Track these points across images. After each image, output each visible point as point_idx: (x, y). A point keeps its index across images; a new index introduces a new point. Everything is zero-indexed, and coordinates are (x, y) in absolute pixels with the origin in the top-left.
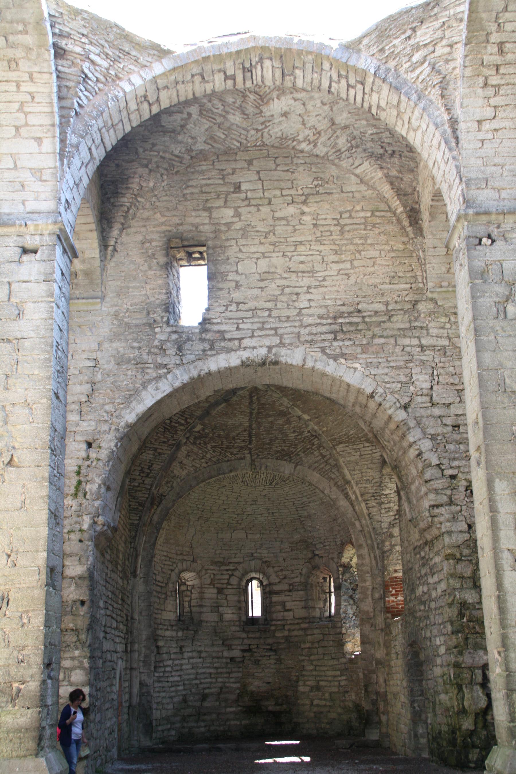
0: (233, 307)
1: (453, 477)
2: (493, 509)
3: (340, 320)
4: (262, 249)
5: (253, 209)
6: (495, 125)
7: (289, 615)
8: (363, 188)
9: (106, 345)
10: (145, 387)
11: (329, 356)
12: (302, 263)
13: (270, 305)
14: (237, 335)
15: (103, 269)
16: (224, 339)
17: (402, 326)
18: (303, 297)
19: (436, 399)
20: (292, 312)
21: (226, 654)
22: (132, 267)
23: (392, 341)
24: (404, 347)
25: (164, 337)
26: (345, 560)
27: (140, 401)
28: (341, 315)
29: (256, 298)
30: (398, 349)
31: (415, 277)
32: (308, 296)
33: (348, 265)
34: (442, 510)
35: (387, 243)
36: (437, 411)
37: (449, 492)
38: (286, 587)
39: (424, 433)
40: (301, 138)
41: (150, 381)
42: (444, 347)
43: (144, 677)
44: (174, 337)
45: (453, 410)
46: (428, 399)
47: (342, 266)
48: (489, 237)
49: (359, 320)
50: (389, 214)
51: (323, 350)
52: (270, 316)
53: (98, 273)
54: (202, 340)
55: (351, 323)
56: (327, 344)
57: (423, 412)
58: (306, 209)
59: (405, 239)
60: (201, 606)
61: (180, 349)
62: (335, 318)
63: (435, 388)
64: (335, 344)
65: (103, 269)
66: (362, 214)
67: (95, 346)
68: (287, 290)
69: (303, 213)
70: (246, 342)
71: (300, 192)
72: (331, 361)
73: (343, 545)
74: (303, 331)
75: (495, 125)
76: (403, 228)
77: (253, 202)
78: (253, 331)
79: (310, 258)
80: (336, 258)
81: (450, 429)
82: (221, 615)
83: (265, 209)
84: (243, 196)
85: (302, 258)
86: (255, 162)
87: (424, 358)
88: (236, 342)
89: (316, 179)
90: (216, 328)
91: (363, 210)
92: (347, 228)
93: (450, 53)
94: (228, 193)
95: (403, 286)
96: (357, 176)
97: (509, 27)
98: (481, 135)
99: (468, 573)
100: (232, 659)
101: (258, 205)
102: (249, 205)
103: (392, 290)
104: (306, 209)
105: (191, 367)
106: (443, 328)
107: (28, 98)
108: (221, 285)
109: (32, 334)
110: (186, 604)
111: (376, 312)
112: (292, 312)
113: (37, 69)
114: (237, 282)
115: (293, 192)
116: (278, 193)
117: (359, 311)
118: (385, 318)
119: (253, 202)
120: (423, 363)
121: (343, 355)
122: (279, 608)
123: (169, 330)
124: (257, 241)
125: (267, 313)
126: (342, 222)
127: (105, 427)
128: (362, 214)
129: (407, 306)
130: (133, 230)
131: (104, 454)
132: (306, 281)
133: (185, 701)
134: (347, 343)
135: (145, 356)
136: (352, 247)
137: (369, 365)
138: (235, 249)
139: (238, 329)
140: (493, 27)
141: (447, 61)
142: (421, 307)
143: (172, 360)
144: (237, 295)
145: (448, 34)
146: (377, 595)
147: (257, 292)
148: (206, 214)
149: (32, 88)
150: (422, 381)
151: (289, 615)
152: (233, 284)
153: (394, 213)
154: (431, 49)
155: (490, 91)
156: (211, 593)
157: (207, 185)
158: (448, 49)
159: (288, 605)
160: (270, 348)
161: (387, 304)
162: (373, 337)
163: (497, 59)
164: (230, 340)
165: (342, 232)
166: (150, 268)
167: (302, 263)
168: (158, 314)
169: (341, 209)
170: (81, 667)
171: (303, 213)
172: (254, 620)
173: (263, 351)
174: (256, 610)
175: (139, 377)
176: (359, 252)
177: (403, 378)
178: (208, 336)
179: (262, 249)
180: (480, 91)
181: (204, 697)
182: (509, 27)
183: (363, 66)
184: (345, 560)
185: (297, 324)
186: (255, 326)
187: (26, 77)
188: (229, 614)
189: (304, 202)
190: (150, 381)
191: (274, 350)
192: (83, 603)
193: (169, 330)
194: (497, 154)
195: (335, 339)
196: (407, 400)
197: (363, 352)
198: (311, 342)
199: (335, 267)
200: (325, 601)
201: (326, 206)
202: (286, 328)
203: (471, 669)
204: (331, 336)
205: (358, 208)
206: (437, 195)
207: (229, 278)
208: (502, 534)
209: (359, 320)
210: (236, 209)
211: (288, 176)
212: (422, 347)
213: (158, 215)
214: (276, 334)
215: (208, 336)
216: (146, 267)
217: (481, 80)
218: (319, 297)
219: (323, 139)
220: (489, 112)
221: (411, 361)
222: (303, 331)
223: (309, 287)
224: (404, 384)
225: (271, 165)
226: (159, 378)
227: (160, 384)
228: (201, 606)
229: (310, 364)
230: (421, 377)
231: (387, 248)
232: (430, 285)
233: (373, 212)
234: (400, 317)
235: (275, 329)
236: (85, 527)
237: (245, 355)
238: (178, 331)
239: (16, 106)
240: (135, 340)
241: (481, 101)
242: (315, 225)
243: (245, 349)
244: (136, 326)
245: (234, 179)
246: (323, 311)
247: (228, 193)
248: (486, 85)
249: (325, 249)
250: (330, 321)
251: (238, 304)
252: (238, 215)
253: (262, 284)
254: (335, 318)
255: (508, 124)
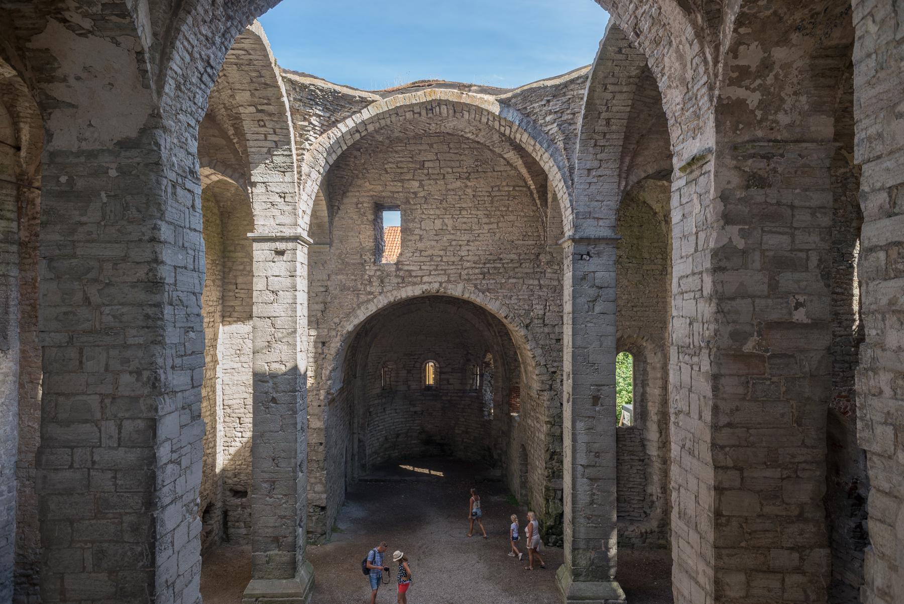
0: (417, 254)
1: (554, 372)
2: (574, 440)
3: (488, 265)
4: (438, 212)
5: (432, 182)
6: (599, 172)
7: (451, 387)
8: (508, 168)
9: (333, 277)
10: (359, 308)
11: (480, 290)
12: (465, 223)
13: (442, 253)
14: (420, 273)
15: (331, 222)
16: (411, 276)
17: (528, 271)
18: (463, 248)
19: (547, 322)
20: (456, 259)
21: (412, 409)
22: (350, 221)
23: (521, 281)
24: (529, 285)
25: (372, 273)
26: (486, 360)
27: (357, 317)
28: (489, 262)
29: (432, 247)
30: (525, 287)
31: (539, 236)
32: (468, 248)
33: (495, 226)
34: (545, 393)
35: (522, 211)
36: (546, 330)
37: (550, 382)
38: (450, 370)
39: (538, 344)
40: (467, 130)
41: (362, 303)
42: (555, 286)
43: (361, 436)
44: (378, 273)
45: (557, 329)
46: (541, 321)
47: (491, 226)
48: (588, 254)
49: (500, 265)
50: (525, 189)
51: (476, 286)
52: (441, 261)
53: (327, 225)
54: (397, 276)
55: (495, 268)
56: (478, 282)
57: (538, 330)
58: (469, 184)
59: (534, 208)
60: (397, 382)
61: (382, 282)
62: (485, 264)
63: (547, 314)
64: (484, 282)
65: (331, 222)
66: (506, 189)
67: (325, 277)
68: (454, 243)
69: (466, 186)
70: (425, 279)
71: (465, 170)
72: (481, 294)
73: (487, 351)
74: (464, 273)
75: (599, 172)
76: (534, 200)
77: (433, 177)
78: (430, 271)
79: (469, 220)
80: (487, 220)
81: (554, 341)
82: (409, 387)
83: (441, 182)
84: (426, 171)
85: (465, 220)
86: (435, 146)
87: (541, 293)
88: (419, 279)
89: (477, 160)
90: (406, 268)
91: (507, 185)
92: (496, 199)
93: (572, 119)
94: (415, 170)
95: (531, 242)
96: (504, 159)
97: (615, 109)
98: (589, 180)
99: (558, 434)
100: (415, 412)
101: (435, 179)
102: (429, 179)
103: (523, 245)
104: (469, 184)
105: (389, 294)
106: (555, 273)
107: (273, 145)
108: (409, 238)
109: (283, 314)
110: (388, 380)
111: (512, 260)
112: (456, 259)
113: (278, 126)
114: (421, 236)
115: (460, 170)
116: (450, 170)
117: (501, 259)
118: (517, 265)
119: (433, 177)
120: (540, 297)
121: (488, 290)
122: (445, 382)
123: (375, 268)
124: (434, 207)
125: (439, 259)
126: (493, 194)
127: (333, 333)
128: (506, 189)
129: (533, 257)
130: (350, 194)
131: (333, 351)
132: (465, 237)
133: (386, 439)
134: (492, 281)
135: (359, 286)
136: (498, 213)
137: (505, 297)
138: (419, 211)
139: (421, 269)
140: (604, 108)
141: (570, 124)
142: (541, 257)
143: (375, 288)
144: (420, 245)
145: (572, 106)
146: (504, 393)
147: (433, 243)
148: (400, 184)
149: (276, 138)
150: (539, 310)
151: (451, 387)
152: (418, 237)
153: (529, 188)
154: (559, 115)
155: (598, 149)
156: (403, 373)
157: (401, 162)
158: (570, 117)
159: (451, 381)
160: (441, 283)
161: (520, 255)
162: (509, 277)
163: (605, 129)
164: (416, 277)
165: (492, 202)
166: (362, 222)
167: (465, 223)
168: (368, 257)
169: (493, 184)
170: (321, 482)
171: (466, 186)
172: (429, 388)
173: (436, 286)
174: (430, 379)
175: (355, 300)
176: (503, 216)
177: (527, 307)
178: (401, 273)
179: (438, 212)
180: (591, 149)
181: (398, 436)
182: (615, 109)
183: (510, 119)
184: (486, 360)
185: (460, 267)
186: (431, 268)
187: (271, 131)
188: (414, 386)
189: (468, 178)
190: (362, 303)
191: (444, 285)
192: (321, 444)
193: (375, 268)
194: (599, 193)
195: (484, 278)
196: (528, 321)
197: (501, 288)
198: (469, 280)
199: (486, 227)
200: (473, 379)
201: (482, 181)
202: (452, 270)
203: (555, 490)
204: (481, 276)
205: (504, 184)
206: (555, 195)
207: (416, 232)
208: (578, 455)
209: (500, 265)
210: (421, 181)
211: (457, 157)
212: (540, 286)
213: (367, 184)
214: (445, 274)
215: (401, 273)
216: (359, 222)
217: (593, 141)
218: (475, 248)
219: (482, 133)
220: (596, 164)
221: (533, 295)
222: (464, 273)
223: (468, 241)
224: (528, 312)
225: (445, 148)
226: (368, 301)
227: (369, 306)
228: (397, 382)
229: (466, 296)
230: (538, 307)
231: (522, 214)
232: (549, 242)
233: (514, 187)
234: (527, 265)
235: (445, 270)
236: (322, 398)
237: (425, 287)
238: (382, 268)
239: (265, 150)
240: (353, 274)
241: (591, 156)
242: (474, 196)
243: (425, 283)
244: (353, 264)
245: (421, 158)
246: (477, 258)
247: (415, 170)
248: (595, 145)
249: (480, 213)
250: (481, 266)
251: (421, 251)
252: (421, 186)
253: (437, 238)
254: (485, 264)
255: (608, 172)
